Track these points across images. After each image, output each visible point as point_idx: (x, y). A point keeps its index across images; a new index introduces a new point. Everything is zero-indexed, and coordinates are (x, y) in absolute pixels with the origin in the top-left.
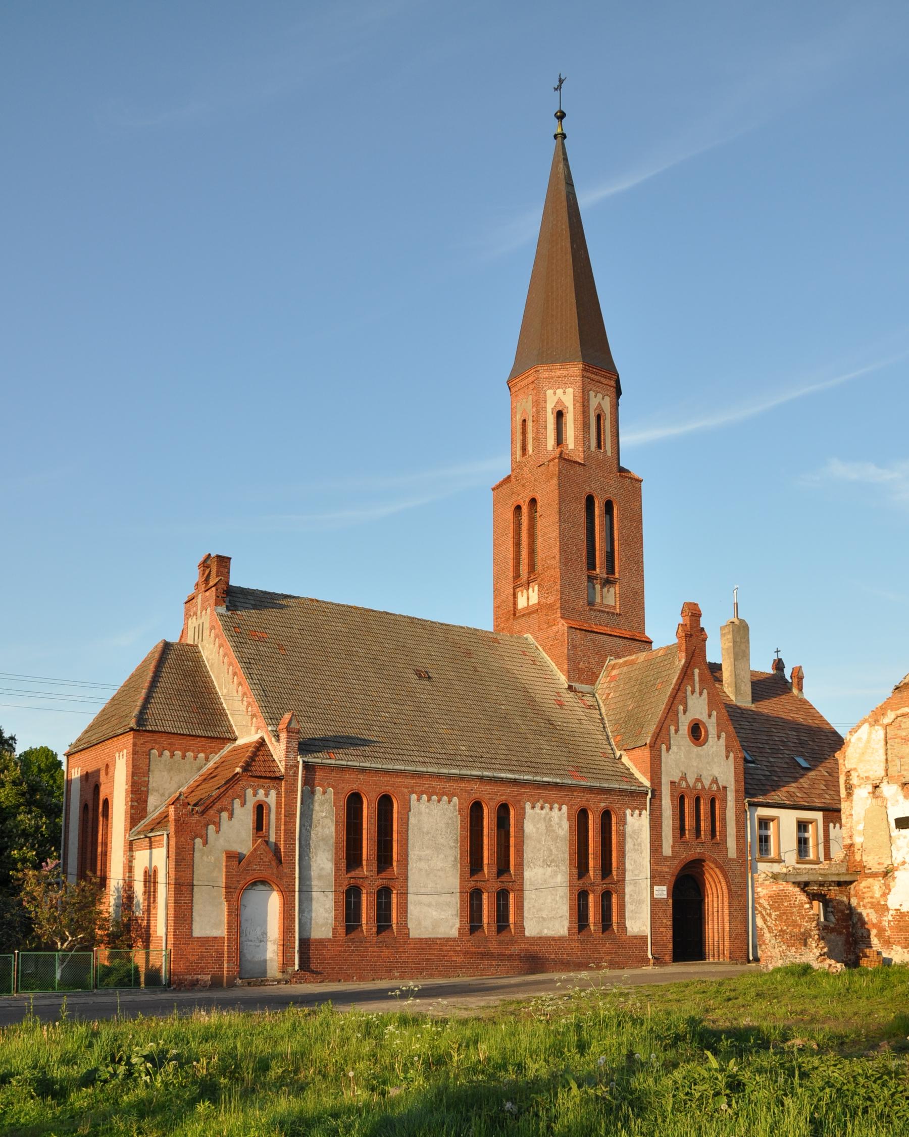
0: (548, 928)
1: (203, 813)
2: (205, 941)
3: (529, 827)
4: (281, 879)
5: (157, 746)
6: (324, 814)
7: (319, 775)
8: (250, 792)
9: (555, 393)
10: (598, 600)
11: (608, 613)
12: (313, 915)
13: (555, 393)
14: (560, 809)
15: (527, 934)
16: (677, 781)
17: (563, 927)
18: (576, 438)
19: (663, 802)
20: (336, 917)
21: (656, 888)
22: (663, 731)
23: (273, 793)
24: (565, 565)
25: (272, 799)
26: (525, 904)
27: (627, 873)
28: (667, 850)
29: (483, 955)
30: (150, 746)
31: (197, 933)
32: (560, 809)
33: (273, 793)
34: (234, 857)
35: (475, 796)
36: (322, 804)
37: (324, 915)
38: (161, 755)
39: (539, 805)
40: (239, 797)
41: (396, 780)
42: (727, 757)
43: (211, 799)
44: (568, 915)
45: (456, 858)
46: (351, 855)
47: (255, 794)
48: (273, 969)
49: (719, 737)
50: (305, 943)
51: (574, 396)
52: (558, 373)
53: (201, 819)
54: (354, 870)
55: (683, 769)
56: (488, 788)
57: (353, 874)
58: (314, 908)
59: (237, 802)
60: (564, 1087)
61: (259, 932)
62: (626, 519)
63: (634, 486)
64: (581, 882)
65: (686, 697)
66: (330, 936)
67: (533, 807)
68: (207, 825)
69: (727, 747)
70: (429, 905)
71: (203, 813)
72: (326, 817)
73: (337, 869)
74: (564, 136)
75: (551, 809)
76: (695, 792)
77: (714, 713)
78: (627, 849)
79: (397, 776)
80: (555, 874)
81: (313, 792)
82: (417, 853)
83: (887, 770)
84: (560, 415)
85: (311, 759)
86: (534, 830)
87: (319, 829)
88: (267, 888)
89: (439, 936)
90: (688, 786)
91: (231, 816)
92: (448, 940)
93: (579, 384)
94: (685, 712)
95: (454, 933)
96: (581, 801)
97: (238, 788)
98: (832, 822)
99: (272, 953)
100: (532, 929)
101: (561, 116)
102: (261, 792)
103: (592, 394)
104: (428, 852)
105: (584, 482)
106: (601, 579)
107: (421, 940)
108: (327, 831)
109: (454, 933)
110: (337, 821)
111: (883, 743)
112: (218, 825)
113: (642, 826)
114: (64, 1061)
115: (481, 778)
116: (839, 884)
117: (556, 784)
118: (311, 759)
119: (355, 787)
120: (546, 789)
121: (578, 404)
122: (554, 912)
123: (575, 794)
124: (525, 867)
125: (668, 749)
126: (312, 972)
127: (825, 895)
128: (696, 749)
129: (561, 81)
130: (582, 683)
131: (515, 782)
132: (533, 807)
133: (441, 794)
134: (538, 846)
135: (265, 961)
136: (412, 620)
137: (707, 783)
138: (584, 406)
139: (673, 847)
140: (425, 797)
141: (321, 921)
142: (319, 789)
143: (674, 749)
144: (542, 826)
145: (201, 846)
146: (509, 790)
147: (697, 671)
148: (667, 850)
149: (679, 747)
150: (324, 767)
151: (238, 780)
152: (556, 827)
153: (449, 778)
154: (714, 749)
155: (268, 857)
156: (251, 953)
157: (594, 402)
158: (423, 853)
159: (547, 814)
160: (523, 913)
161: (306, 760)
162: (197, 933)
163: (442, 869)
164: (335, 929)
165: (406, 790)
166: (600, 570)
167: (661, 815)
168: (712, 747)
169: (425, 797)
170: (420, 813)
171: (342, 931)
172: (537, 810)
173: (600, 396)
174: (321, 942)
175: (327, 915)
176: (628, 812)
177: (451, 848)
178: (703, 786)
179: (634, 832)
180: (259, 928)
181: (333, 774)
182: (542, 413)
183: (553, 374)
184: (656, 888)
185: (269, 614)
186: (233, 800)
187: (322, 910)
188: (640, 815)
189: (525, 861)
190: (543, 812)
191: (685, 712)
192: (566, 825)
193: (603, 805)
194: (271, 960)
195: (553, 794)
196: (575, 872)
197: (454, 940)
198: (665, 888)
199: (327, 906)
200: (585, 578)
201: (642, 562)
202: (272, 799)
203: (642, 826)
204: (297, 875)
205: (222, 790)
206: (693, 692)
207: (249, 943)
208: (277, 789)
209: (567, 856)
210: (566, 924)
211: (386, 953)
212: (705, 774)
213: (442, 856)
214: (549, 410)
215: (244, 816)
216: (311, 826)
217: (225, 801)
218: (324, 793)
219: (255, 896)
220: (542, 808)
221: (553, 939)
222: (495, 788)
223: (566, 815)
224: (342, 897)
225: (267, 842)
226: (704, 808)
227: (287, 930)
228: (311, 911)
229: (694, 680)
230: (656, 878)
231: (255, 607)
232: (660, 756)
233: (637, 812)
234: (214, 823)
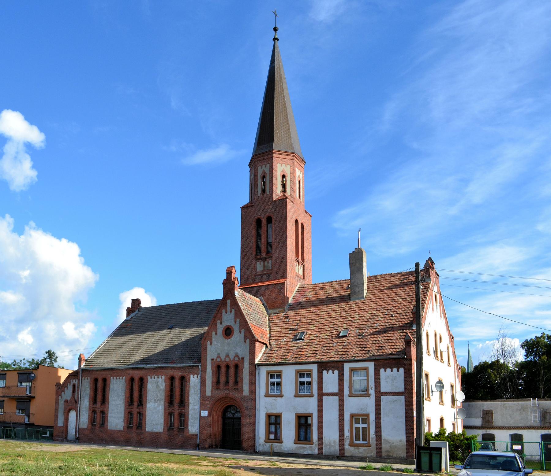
2: (60, 427)
15: (147, 430)
21: (202, 411)
28: (208, 393)
34: (66, 401)
42: (245, 342)
49: (240, 332)
55: (219, 352)
57: (94, 406)
69: (245, 336)
70: (115, 418)
73: (90, 405)
76: (225, 363)
80: (158, 406)
84: (299, 182)
90: (221, 360)
92: (120, 431)
96: (171, 373)
98: (325, 369)
101: (275, 29)
103: (259, 168)
104: (116, 398)
107: (113, 431)
109: (122, 428)
112: (64, 391)
114: (212, 445)
125: (211, 344)
129: (275, 13)
131: (143, 368)
133: (119, 376)
137: (232, 357)
139: (211, 391)
143: (214, 343)
144: (155, 385)
148: (208, 393)
152: (160, 386)
154: (238, 339)
155: (73, 401)
176: (192, 376)
178: (230, 359)
184: (202, 411)
192: (164, 384)
195: (159, 371)
196: (167, 405)
198: (207, 412)
202: (76, 383)
226: (232, 370)
230: (203, 407)
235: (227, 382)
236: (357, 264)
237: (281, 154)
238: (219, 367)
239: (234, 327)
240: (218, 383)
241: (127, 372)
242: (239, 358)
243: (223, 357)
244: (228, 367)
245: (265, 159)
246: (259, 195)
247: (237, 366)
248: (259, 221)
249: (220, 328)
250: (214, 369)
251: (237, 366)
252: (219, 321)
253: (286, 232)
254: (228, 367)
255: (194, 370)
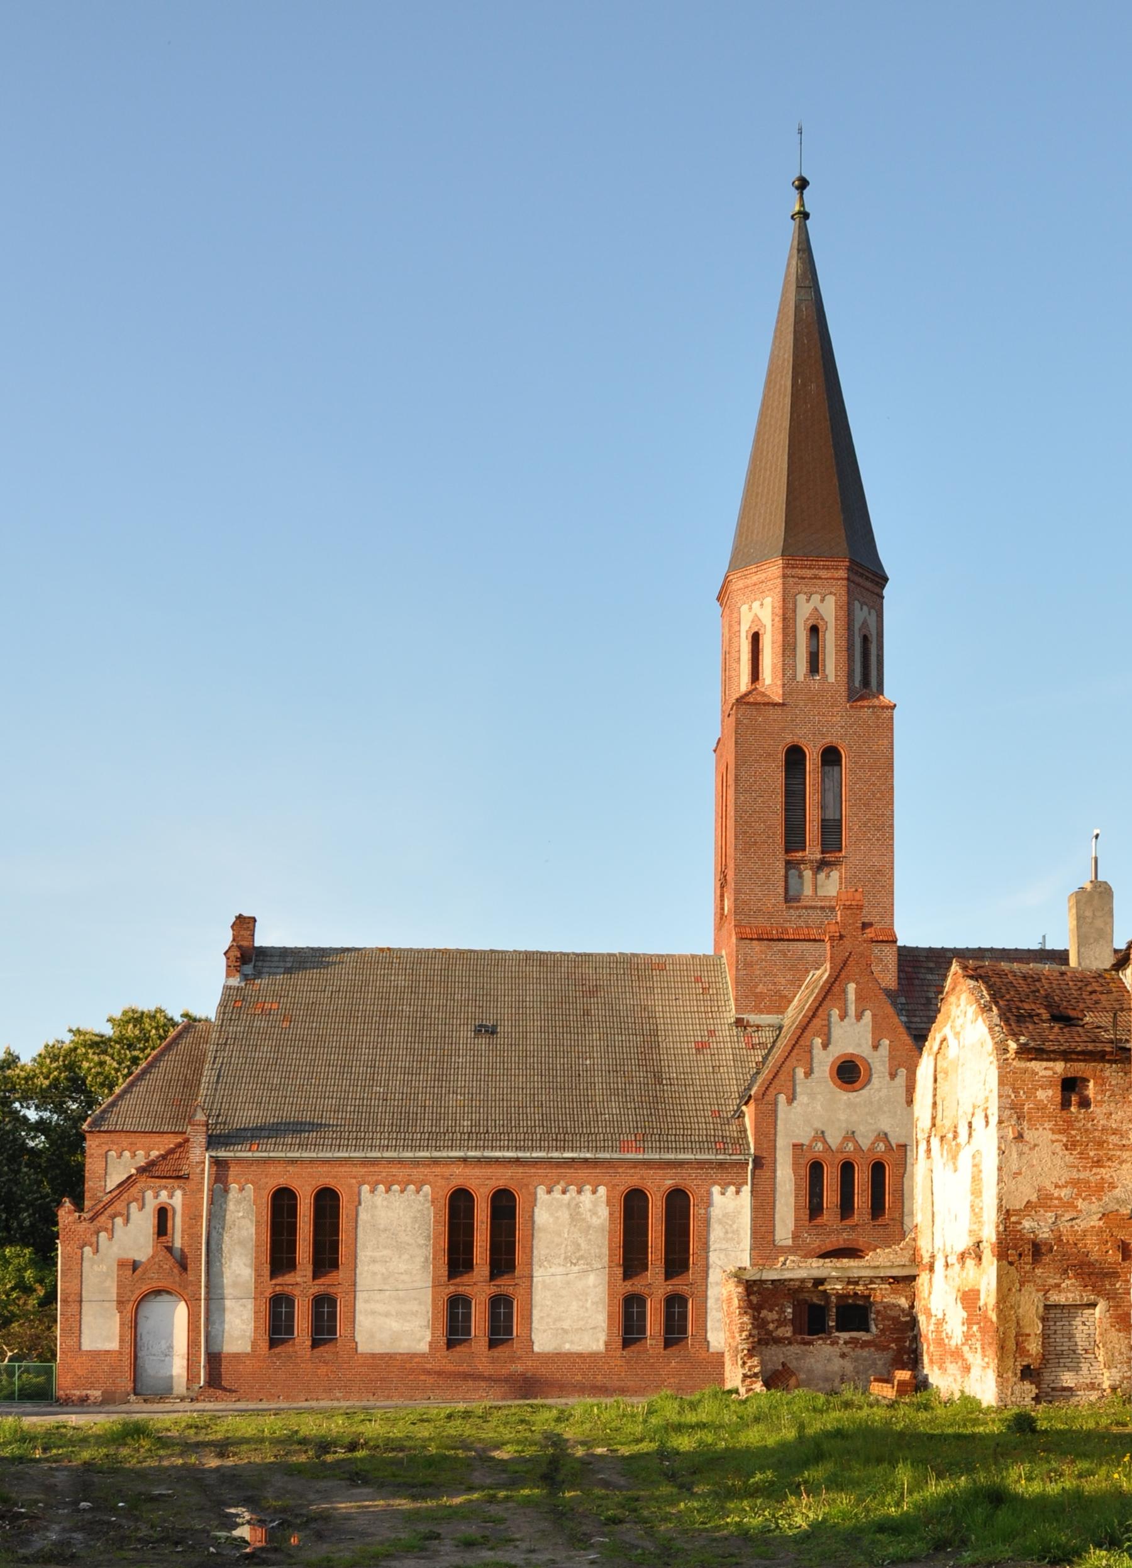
0: (572, 1342)
1: (92, 1219)
2: (95, 1355)
3: (542, 1216)
4: (185, 1288)
5: (115, 1147)
6: (241, 1214)
7: (233, 1171)
8: (149, 1194)
9: (750, 608)
10: (808, 891)
11: (822, 908)
12: (227, 1327)
13: (750, 608)
14: (594, 1192)
15: (536, 1349)
16: (806, 1142)
17: (598, 1341)
18: (774, 666)
19: (779, 1173)
20: (256, 1328)
22: (782, 1076)
23: (178, 1194)
24: (745, 852)
25: (177, 1200)
26: (535, 1312)
27: (711, 1271)
29: (466, 1376)
30: (106, 1148)
31: (86, 1346)
32: (594, 1192)
33: (178, 1194)
35: (456, 1183)
36: (238, 1202)
37: (240, 1326)
38: (120, 1156)
39: (559, 1188)
40: (136, 1200)
41: (340, 1169)
43: (102, 1205)
44: (605, 1325)
45: (427, 1259)
46: (280, 1257)
47: (157, 1196)
48: (180, 1386)
49: (893, 1076)
50: (214, 1359)
51: (773, 608)
52: (755, 578)
53: (91, 1226)
54: (284, 1275)
56: (477, 1171)
57: (279, 1280)
58: (227, 1319)
59: (134, 1206)
60: (53, 1476)
61: (164, 1345)
62: (861, 767)
63: (878, 718)
64: (629, 1283)
65: (829, 1026)
66: (249, 1349)
67: (549, 1192)
68: (97, 1233)
70: (387, 1315)
71: (92, 1219)
72: (243, 1217)
73: (258, 1275)
74: (805, 215)
75: (579, 1192)
76: (841, 1156)
77: (886, 1042)
78: (712, 1237)
79: (341, 1165)
81: (226, 1191)
82: (368, 1254)
83: (934, 1118)
84: (756, 638)
85: (222, 1154)
86: (551, 1220)
87: (235, 1231)
88: (173, 1298)
89: (401, 1351)
90: (858, 1148)
91: (127, 1220)
93: (779, 589)
94: (825, 1046)
95: (423, 1347)
97: (134, 1191)
99: (178, 1368)
100: (544, 1340)
101: (802, 184)
102: (164, 1194)
103: (801, 598)
104: (386, 1252)
105: (783, 729)
106: (811, 861)
108: (244, 1233)
109: (423, 1347)
110: (257, 1221)
111: (932, 1079)
112: (111, 1233)
113: (742, 1207)
115: (465, 1160)
116: (896, 1280)
117: (586, 1160)
118: (222, 1154)
119: (282, 1182)
120: (570, 1168)
121: (777, 619)
122: (581, 1323)
123: (620, 1170)
124: (535, 1267)
125: (791, 1100)
126: (225, 1389)
127: (869, 1296)
128: (845, 1097)
130: (761, 1012)
131: (517, 1160)
132: (549, 1192)
134: (557, 1240)
135: (171, 1377)
136: (529, 957)
138: (784, 619)
140: (381, 1188)
141: (236, 1333)
142: (234, 1187)
143: (802, 1098)
144: (564, 1215)
145: (91, 1255)
146: (509, 1172)
147: (851, 987)
149: (812, 1096)
150: (239, 1161)
151: (135, 1182)
153: (416, 1163)
154: (884, 1092)
155: (169, 1264)
156: (151, 1367)
157: (804, 610)
158: (377, 1254)
159: (573, 1198)
160: (531, 1323)
161: (213, 1154)
162: (86, 1346)
163: (406, 1272)
164: (254, 1344)
165: (354, 1181)
166: (813, 851)
167: (774, 1190)
168: (879, 1090)
169: (381, 1188)
170: (374, 1207)
171: (264, 1345)
172: (557, 1194)
173: (816, 598)
174: (236, 1356)
175: (244, 1327)
176: (716, 1190)
177: (419, 1246)
179: (726, 1215)
180: (163, 1342)
181: (254, 1168)
182: (735, 640)
183: (749, 582)
185: (304, 979)
186: (128, 1205)
187: (238, 1321)
188: (738, 1192)
189: (535, 1260)
190: (567, 1196)
191: (825, 1046)
192: (604, 1212)
193: (669, 1182)
194: (179, 1376)
195: (583, 1173)
197: (423, 1355)
199: (245, 1317)
200: (780, 866)
201: (892, 826)
203: (742, 1207)
204: (203, 1284)
205: (114, 1194)
206: (843, 1017)
207: (152, 1358)
208: (184, 1189)
209: (605, 1251)
210: (602, 1337)
211: (323, 1369)
212: (861, 1130)
213: (406, 1257)
214: (743, 635)
215: (143, 1221)
216: (223, 1228)
217: (119, 1206)
218: (242, 1189)
219: (156, 1309)
220: (564, 1192)
221: (580, 1355)
222: (488, 1171)
223: (604, 1199)
224: (264, 1307)
225: (169, 1249)
227: (192, 1344)
228: (223, 1322)
229: (846, 1000)
231: (288, 971)
232: (775, 1111)
233: (732, 1189)
234: (106, 1230)
235: (846, 1207)
236: (1099, 923)
237: (862, 575)
238: (816, 1169)
239: (837, 1055)
240: (815, 1208)
241: (438, 1170)
242: (889, 1147)
243: (834, 1141)
244: (847, 1168)
245: (816, 577)
246: (800, 677)
247: (878, 1169)
248: (795, 757)
249: (824, 1061)
250: (803, 1172)
251: (878, 1169)
252: (818, 1041)
253: (891, 803)
254: (847, 1168)
255: (727, 1171)
